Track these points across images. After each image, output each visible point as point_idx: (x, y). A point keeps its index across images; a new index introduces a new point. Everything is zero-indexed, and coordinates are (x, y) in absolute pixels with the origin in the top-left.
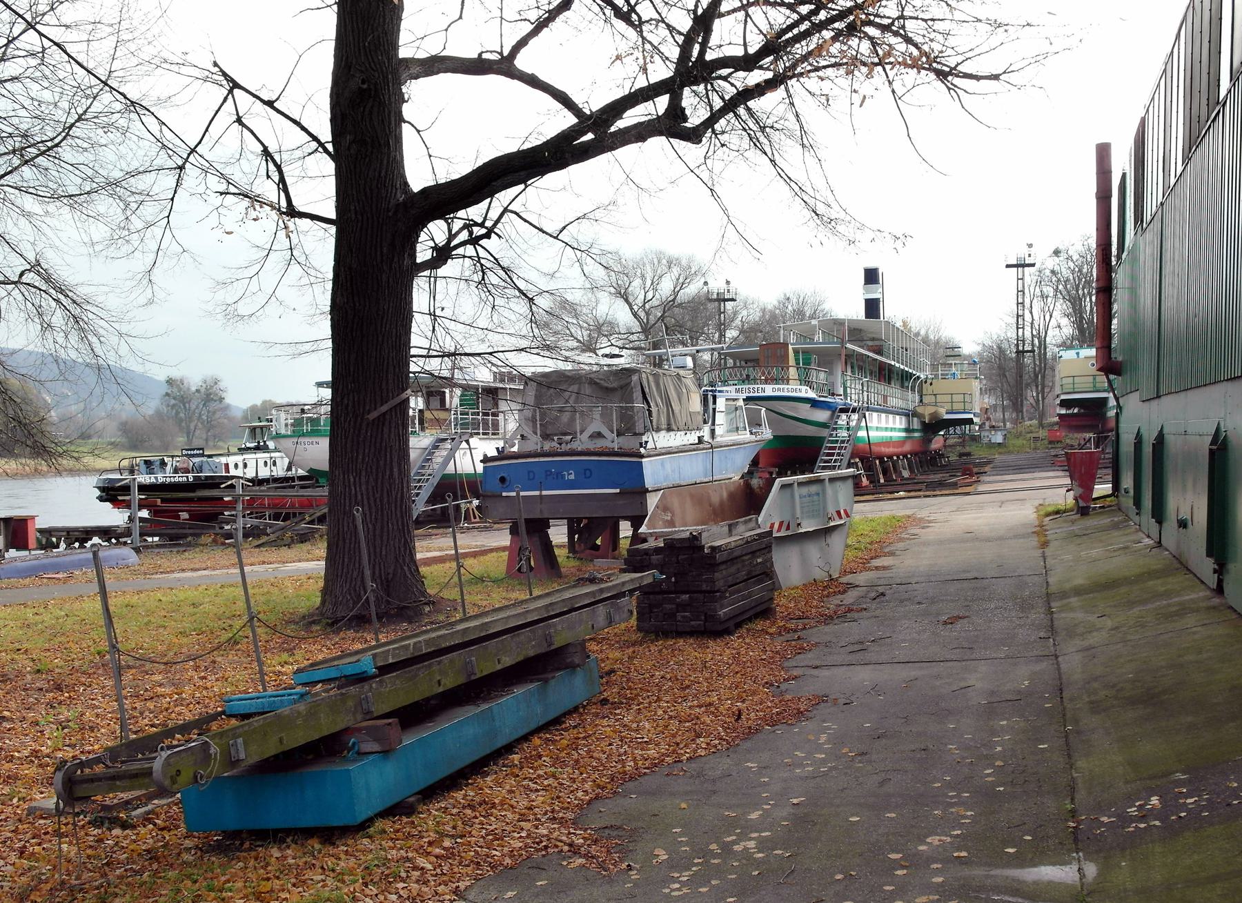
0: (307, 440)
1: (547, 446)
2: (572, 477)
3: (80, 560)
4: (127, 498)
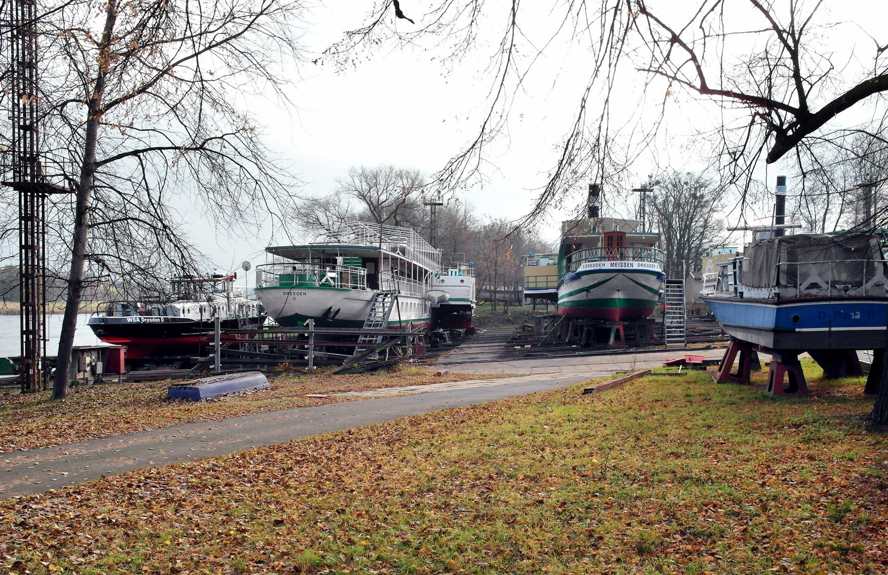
0: (296, 291)
1: (835, 293)
2: (858, 317)
3: (244, 383)
4: (211, 333)
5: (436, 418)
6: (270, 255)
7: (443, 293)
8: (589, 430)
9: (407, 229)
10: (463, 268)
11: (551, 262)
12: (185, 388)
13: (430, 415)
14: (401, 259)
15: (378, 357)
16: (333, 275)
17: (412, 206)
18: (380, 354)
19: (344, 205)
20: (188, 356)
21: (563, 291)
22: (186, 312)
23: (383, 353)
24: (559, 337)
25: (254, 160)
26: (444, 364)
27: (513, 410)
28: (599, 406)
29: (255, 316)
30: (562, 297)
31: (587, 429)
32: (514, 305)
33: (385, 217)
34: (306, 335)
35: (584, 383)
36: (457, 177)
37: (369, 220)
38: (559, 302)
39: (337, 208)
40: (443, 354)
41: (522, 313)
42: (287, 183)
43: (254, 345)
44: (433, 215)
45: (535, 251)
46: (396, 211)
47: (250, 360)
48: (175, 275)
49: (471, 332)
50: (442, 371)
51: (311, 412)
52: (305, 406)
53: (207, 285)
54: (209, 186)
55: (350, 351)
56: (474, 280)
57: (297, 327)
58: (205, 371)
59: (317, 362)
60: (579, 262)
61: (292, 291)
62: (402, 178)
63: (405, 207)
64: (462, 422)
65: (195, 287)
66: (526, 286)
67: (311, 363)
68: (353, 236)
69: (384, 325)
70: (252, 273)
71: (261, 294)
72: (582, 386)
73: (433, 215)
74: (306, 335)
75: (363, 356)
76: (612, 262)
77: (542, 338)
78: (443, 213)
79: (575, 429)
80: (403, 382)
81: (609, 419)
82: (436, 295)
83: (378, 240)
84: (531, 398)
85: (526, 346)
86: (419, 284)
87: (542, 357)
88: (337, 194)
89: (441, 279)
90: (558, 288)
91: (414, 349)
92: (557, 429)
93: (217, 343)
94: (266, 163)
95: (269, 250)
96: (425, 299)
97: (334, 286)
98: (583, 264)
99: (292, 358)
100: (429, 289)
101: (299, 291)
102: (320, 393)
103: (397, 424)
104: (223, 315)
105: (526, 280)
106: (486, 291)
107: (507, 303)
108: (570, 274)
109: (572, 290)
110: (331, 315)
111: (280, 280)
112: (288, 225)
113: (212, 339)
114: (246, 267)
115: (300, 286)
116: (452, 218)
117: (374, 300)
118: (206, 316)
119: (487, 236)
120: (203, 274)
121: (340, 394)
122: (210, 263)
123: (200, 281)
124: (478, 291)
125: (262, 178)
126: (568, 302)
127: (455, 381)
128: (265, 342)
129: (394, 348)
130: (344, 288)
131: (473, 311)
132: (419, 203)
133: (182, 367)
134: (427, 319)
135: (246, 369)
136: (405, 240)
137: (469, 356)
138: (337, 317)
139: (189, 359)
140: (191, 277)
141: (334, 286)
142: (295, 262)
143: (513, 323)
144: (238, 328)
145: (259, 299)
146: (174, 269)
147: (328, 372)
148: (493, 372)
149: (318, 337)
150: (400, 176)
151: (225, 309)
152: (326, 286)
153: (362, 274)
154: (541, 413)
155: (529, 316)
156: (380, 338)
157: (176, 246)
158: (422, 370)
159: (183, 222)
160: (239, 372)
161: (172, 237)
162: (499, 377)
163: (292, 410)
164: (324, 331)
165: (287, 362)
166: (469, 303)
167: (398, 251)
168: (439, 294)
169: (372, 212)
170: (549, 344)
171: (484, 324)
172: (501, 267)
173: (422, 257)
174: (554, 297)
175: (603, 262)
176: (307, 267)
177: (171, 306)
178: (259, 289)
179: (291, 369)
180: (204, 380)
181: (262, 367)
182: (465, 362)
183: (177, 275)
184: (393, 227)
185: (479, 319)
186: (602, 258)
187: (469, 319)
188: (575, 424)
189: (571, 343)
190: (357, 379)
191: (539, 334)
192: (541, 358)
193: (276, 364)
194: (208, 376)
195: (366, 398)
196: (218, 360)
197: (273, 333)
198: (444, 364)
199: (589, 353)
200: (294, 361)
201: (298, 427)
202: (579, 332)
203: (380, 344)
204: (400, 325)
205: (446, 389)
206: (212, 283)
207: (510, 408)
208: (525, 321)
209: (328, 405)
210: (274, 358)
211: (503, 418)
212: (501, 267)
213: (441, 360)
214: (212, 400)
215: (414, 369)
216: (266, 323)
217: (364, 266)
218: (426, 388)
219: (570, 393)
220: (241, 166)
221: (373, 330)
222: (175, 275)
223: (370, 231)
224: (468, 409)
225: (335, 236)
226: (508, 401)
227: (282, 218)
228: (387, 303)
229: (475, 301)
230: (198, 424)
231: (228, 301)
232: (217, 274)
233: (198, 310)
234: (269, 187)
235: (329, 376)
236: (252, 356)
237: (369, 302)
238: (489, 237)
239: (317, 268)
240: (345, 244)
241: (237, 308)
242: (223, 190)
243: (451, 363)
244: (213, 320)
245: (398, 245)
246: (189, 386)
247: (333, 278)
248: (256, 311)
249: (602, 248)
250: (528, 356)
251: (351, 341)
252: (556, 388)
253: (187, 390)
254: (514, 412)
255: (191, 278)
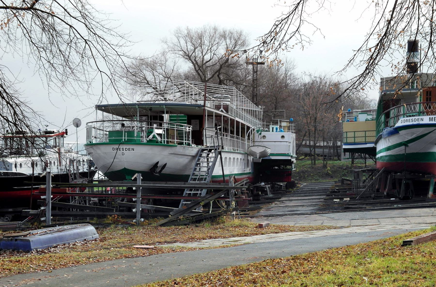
0: (125, 147)
4: (42, 186)
5: (258, 269)
6: (100, 112)
7: (264, 148)
8: (408, 282)
9: (230, 88)
10: (284, 124)
11: (370, 117)
12: (16, 240)
13: (252, 266)
14: (224, 116)
15: (202, 209)
16: (160, 131)
17: (235, 65)
18: (204, 206)
19: (170, 64)
20: (19, 209)
21: (381, 146)
22: (18, 166)
23: (206, 206)
24: (378, 190)
25: (83, 21)
26: (265, 216)
27: (332, 261)
28: (419, 258)
29: (85, 170)
30: (380, 152)
31: (406, 281)
32: (333, 160)
33: (209, 76)
34: (134, 188)
35: (402, 235)
36: (280, 39)
37: (194, 79)
38: (378, 156)
39: (163, 67)
40: (264, 207)
41: (341, 167)
42: (115, 43)
43: (84, 197)
44: (255, 74)
45: (353, 107)
46: (219, 70)
47: (80, 213)
48: (7, 131)
49: (291, 185)
50: (264, 223)
51: (139, 262)
52: (133, 257)
53: (39, 142)
54: (40, 44)
55: (176, 204)
56: (294, 135)
57: (126, 181)
58: (36, 224)
59: (145, 214)
60: (397, 117)
61: (121, 147)
62: (225, 38)
63: (229, 66)
64: (283, 272)
65: (27, 142)
66: (345, 141)
67: (139, 215)
68: (179, 94)
69: (208, 179)
70: (82, 130)
71: (91, 150)
72: (401, 238)
73: (255, 74)
74: (134, 188)
75: (189, 209)
76: (431, 117)
77: (361, 192)
78: (264, 71)
79: (394, 281)
80: (226, 233)
81: (428, 271)
82: (258, 150)
83: (203, 98)
84: (350, 250)
85: (345, 199)
86: (242, 140)
87: (361, 209)
88: (164, 54)
89: (262, 135)
90: (376, 143)
91: (237, 203)
92: (375, 280)
93: (49, 197)
94: (94, 23)
95: (99, 107)
96: (248, 154)
97: (161, 142)
98: (402, 119)
99: (120, 211)
100: (251, 144)
101: (128, 147)
102: (147, 244)
103: (220, 275)
104: (54, 170)
105: (345, 135)
106: (306, 146)
107: (325, 157)
108: (389, 129)
109: (390, 144)
110: (158, 170)
111: (109, 137)
112: (117, 83)
113: (44, 192)
114: (77, 124)
115: (128, 142)
116: (274, 77)
117: (199, 155)
118: (38, 171)
119: (307, 94)
120: (35, 130)
121: (166, 246)
122: (42, 120)
123: (31, 137)
124: (299, 146)
125: (91, 38)
126: (386, 156)
127: (276, 233)
128: (94, 195)
129: (218, 201)
130: (170, 144)
131: (293, 165)
132: (241, 63)
133: (14, 219)
134: (250, 173)
135: (76, 221)
136: (227, 98)
137: (290, 209)
138: (164, 171)
139: (21, 212)
140: (23, 133)
141: (161, 142)
142: (124, 119)
143: (332, 177)
144: (69, 182)
145: (89, 154)
146: (7, 125)
147: (155, 224)
148: (313, 224)
149: (146, 190)
150: (223, 36)
151: (56, 164)
152: (153, 142)
153: (188, 130)
154: (360, 264)
155: (348, 170)
156: (204, 192)
157: (8, 103)
158: (245, 222)
159: (16, 81)
160: (69, 224)
161: (5, 95)
162: (318, 229)
163: (120, 261)
164: (151, 184)
165: (115, 214)
166: (290, 158)
167: (222, 109)
168: (261, 150)
169: (197, 71)
170: (368, 197)
171: (304, 178)
172: (320, 123)
173: (244, 114)
174: (372, 152)
175: (422, 117)
176: (135, 124)
177: (3, 161)
178: (90, 145)
179: (119, 221)
180: (35, 232)
181: (92, 219)
182: (286, 215)
183: (10, 131)
184: (217, 85)
185: (299, 173)
186: (420, 113)
187: (289, 173)
188: (395, 276)
189: (389, 196)
190: (182, 230)
191: (358, 187)
192: (360, 211)
193: (105, 216)
194: (39, 228)
195: (191, 249)
196: (49, 213)
197: (102, 187)
198: (265, 216)
199: (404, 206)
200: (123, 213)
201: (126, 277)
202: (397, 186)
203: (204, 197)
204: (224, 179)
205: (267, 240)
206: (44, 139)
207: (330, 259)
208: (345, 175)
209: (154, 256)
210: (103, 210)
211: (322, 269)
212: (320, 123)
213: (263, 212)
214: (43, 252)
215: (237, 221)
216: (96, 177)
217: (189, 123)
218: (248, 239)
219: (389, 245)
220: (71, 26)
221: (197, 184)
222: (7, 131)
223: (196, 90)
224: (288, 260)
225: (162, 95)
226: (327, 253)
227: (111, 77)
228: (211, 158)
229: (295, 155)
230: (28, 275)
231: (60, 157)
232: (49, 130)
233: (30, 165)
234: (98, 47)
235: (156, 228)
236: (82, 209)
237: (194, 157)
238: (309, 95)
239: (144, 125)
240: (171, 102)
241: (68, 163)
242: (54, 49)
243: (272, 216)
244: (44, 174)
245: (222, 103)
246: (20, 238)
247: (160, 135)
248: (86, 166)
249: (420, 103)
250: (347, 208)
251: (177, 194)
252: (374, 239)
253: (18, 242)
254: (334, 263)
255: (23, 134)
